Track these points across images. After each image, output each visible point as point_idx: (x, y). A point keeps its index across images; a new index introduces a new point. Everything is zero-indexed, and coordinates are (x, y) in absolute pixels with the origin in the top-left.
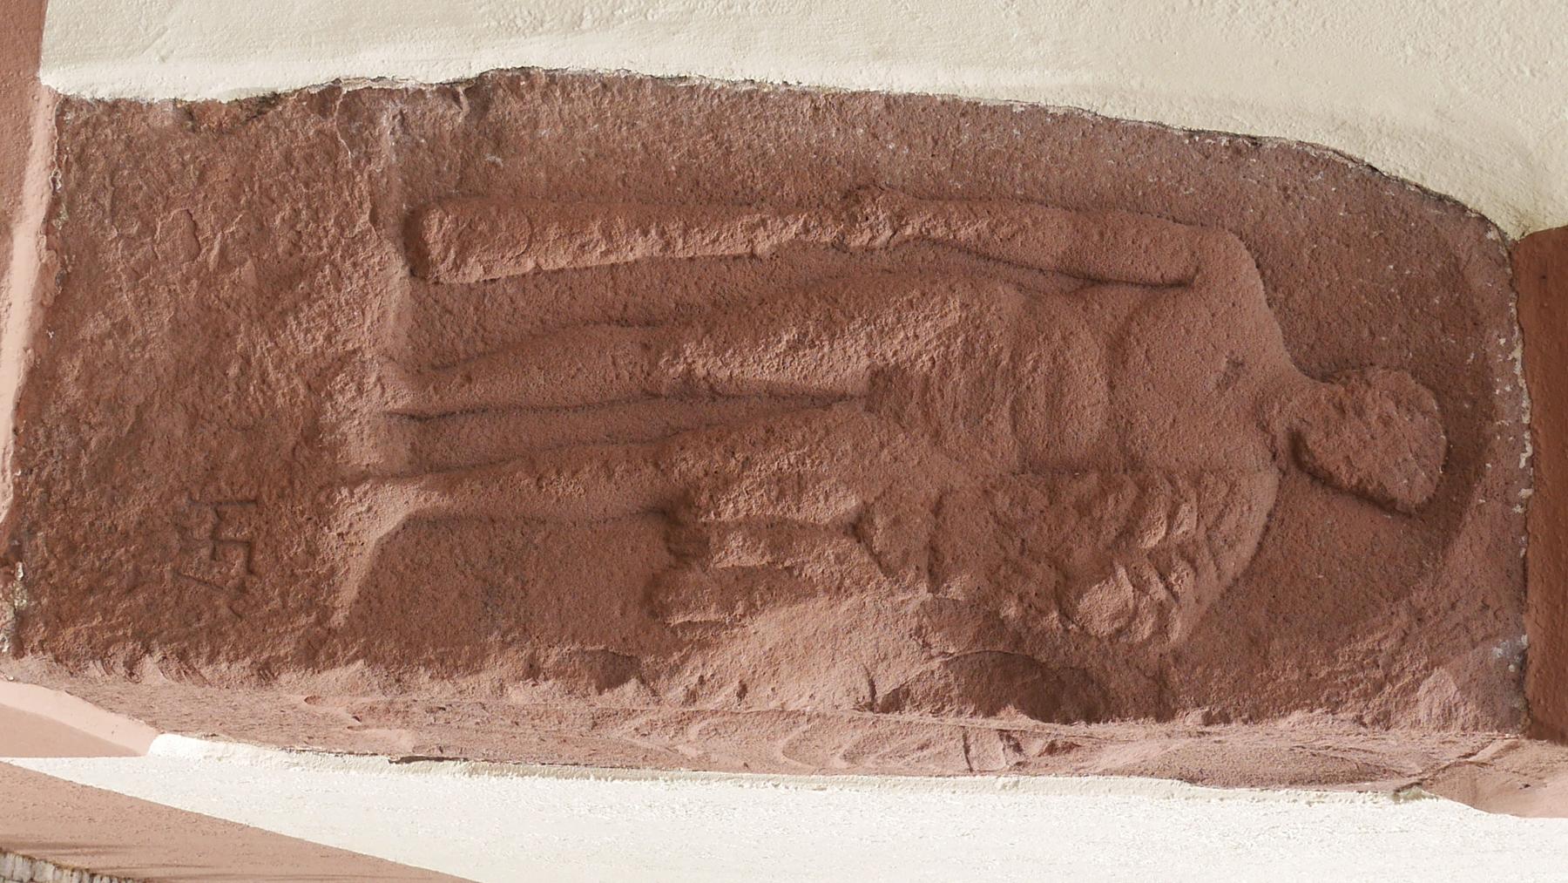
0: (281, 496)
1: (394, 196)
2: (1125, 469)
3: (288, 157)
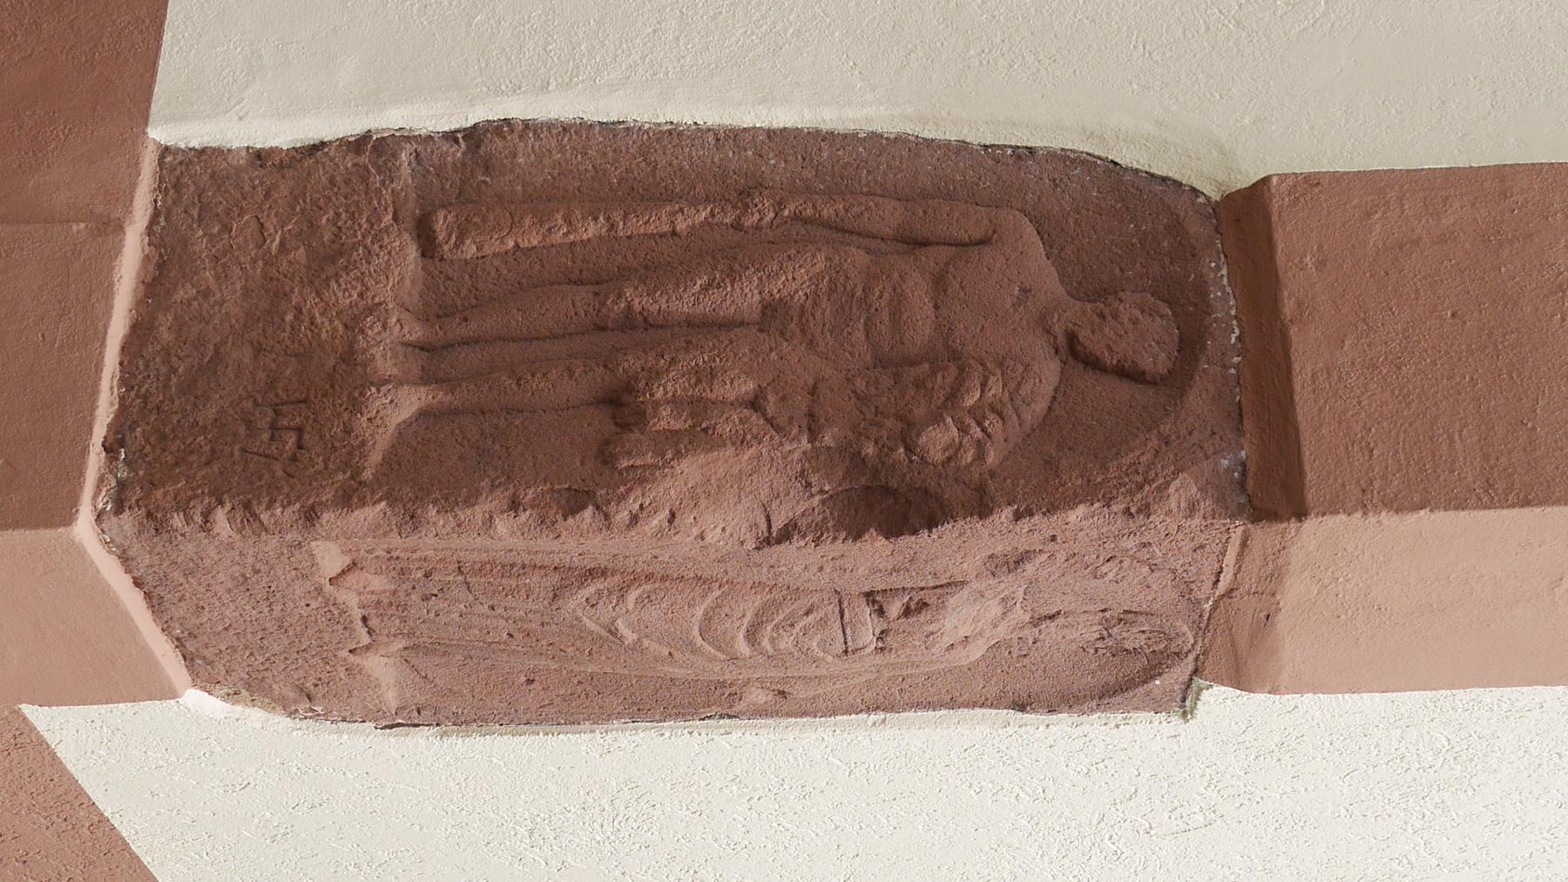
0: (325, 395)
1: (411, 204)
2: (949, 356)
3: (332, 182)
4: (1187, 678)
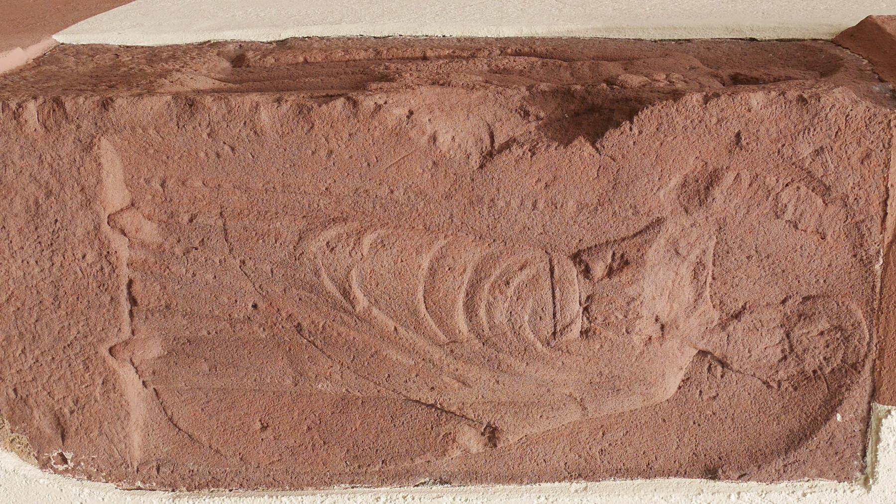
4: (865, 406)
